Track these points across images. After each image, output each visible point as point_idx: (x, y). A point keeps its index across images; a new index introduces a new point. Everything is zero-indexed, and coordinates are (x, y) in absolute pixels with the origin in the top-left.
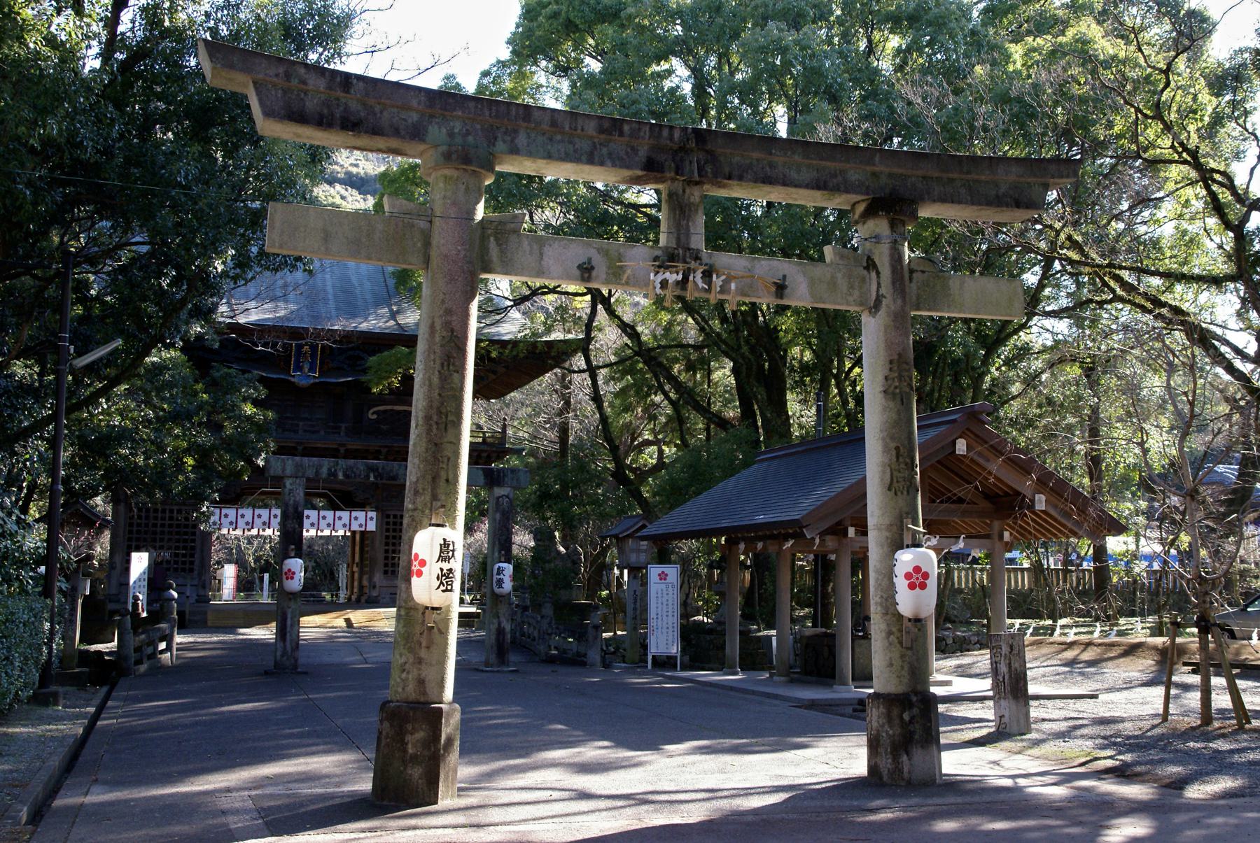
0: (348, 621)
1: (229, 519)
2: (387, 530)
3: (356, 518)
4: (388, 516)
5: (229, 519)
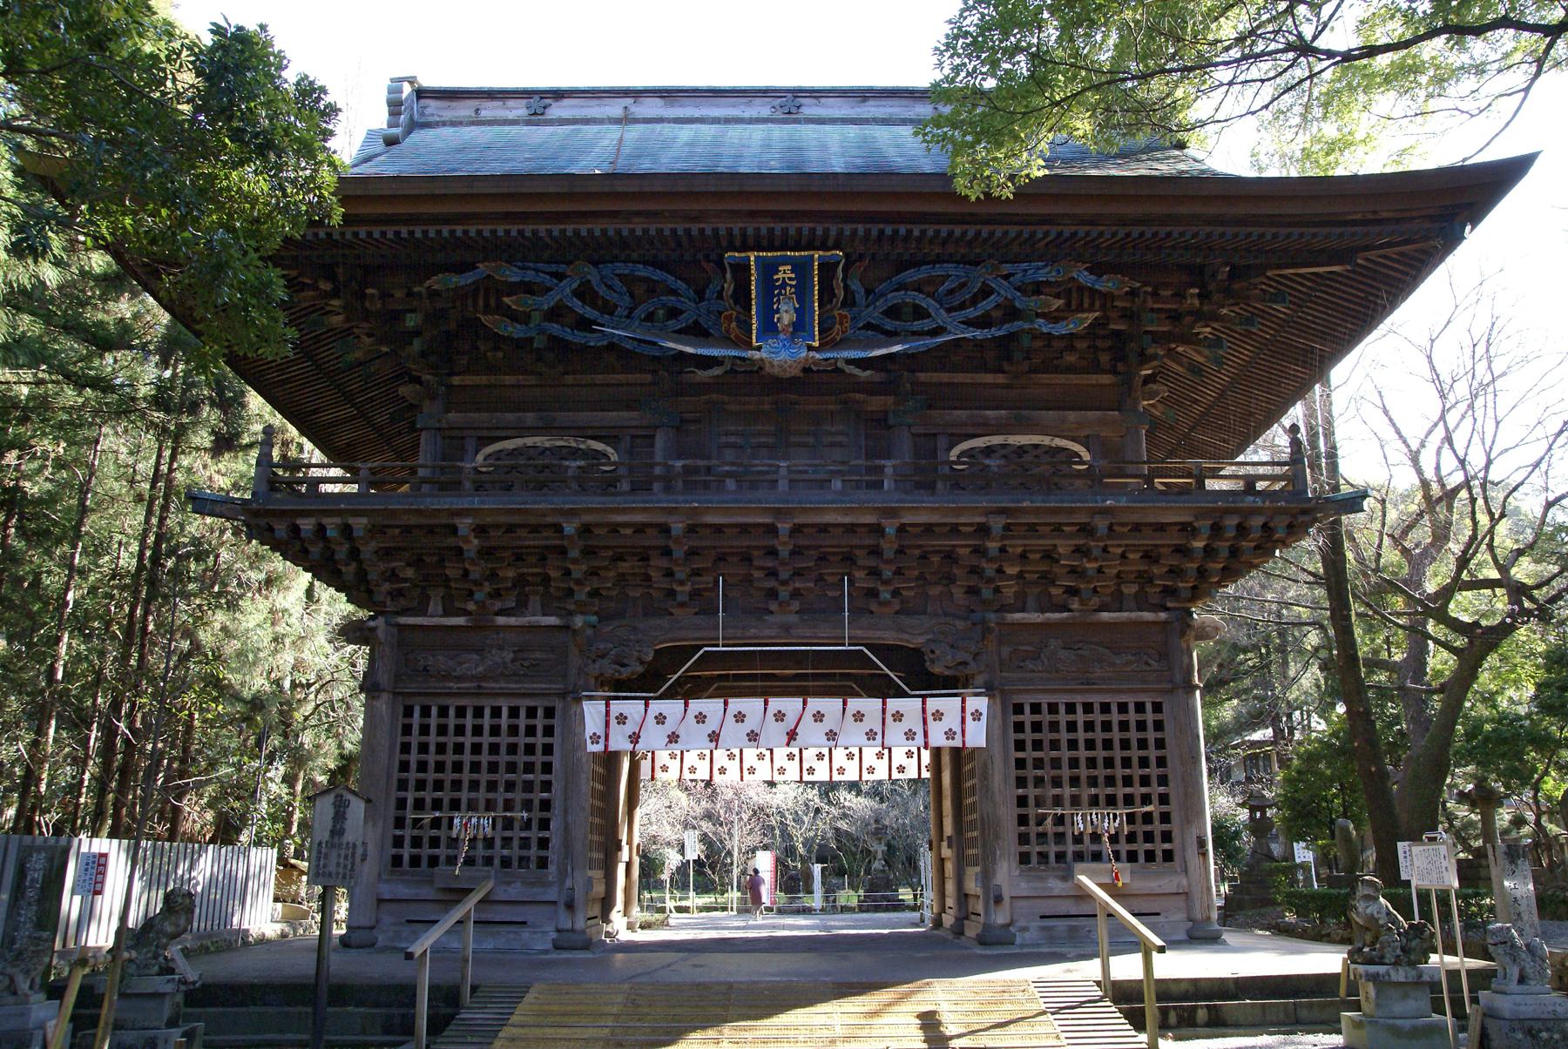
2: (1020, 745)
4: (1019, 709)
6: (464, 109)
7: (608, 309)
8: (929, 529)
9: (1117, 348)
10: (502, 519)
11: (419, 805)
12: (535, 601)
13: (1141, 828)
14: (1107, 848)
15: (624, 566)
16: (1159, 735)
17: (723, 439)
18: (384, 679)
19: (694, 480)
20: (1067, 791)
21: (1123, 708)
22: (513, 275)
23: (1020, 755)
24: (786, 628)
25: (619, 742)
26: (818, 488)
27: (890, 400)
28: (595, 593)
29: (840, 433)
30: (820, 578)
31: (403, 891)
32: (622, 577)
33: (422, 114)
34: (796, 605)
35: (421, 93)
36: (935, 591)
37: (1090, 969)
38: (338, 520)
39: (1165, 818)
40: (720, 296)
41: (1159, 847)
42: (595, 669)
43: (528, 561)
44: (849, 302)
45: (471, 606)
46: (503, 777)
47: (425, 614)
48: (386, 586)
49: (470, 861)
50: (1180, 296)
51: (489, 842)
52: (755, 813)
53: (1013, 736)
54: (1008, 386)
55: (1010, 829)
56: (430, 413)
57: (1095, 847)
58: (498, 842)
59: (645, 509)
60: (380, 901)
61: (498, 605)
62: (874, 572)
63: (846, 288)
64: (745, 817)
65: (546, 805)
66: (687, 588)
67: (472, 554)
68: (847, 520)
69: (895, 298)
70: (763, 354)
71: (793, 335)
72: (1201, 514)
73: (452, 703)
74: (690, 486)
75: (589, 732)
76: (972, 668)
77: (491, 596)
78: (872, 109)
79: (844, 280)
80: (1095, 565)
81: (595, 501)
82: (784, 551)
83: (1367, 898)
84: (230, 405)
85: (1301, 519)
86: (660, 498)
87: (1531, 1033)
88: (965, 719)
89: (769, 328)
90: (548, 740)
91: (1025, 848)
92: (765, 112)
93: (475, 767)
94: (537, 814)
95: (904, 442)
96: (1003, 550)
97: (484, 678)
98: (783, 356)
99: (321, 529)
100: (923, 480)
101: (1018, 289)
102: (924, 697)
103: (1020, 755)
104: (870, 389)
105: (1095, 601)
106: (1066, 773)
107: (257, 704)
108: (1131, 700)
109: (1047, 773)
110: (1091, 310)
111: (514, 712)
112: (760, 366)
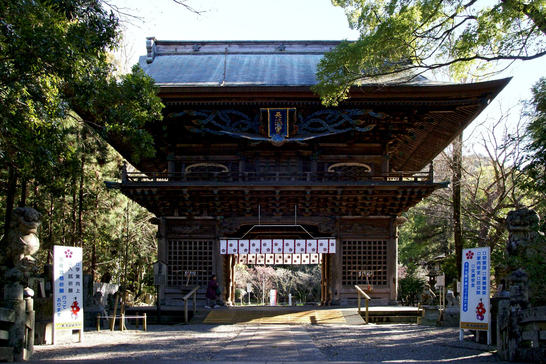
0: (313, 319)
1: (244, 247)
2: (344, 253)
3: (321, 244)
4: (345, 243)
5: (244, 247)
6: (171, 49)
7: (224, 124)
8: (320, 192)
9: (382, 136)
10: (196, 189)
11: (175, 268)
12: (205, 212)
13: (377, 276)
14: (368, 281)
15: (231, 202)
16: (385, 250)
17: (260, 164)
18: (163, 234)
19: (251, 178)
20: (357, 265)
21: (375, 243)
22: (195, 113)
23: (344, 255)
24: (278, 220)
25: (230, 251)
26: (287, 180)
27: (311, 152)
28: (222, 210)
29: (295, 162)
30: (288, 206)
31: (172, 291)
32: (230, 205)
33: (158, 51)
34: (281, 213)
35: (157, 43)
36: (322, 209)
37: (357, 309)
38: (148, 189)
39: (385, 273)
40: (258, 120)
41: (383, 281)
42: (223, 231)
43: (202, 201)
44: (298, 122)
45: (187, 214)
46: (198, 261)
47: (173, 216)
48: (162, 208)
49: (190, 283)
50: (402, 119)
51: (195, 278)
52: (270, 278)
53: (342, 250)
54: (348, 148)
55: (340, 276)
56: (170, 156)
57: (364, 280)
58: (198, 278)
59: (238, 186)
60: (166, 293)
61: (195, 213)
62: (304, 204)
63: (298, 118)
64: (267, 280)
65: (211, 268)
66: (250, 208)
67: (187, 199)
68: (296, 189)
69: (313, 120)
70: (272, 140)
71: (281, 134)
72: (401, 188)
73: (183, 241)
74: (250, 180)
75: (221, 248)
76: (332, 231)
77: (192, 211)
78: (309, 49)
79: (297, 115)
80: (368, 202)
81: (223, 184)
82: (278, 198)
83: (426, 289)
84: (103, 150)
85: (430, 189)
86: (241, 183)
87: (452, 316)
88: (329, 246)
89: (274, 131)
90: (210, 251)
91: (344, 280)
92: (273, 50)
93: (190, 258)
94: (208, 271)
95: (314, 166)
96: (341, 198)
97: (191, 234)
98: (278, 140)
99: (143, 192)
100: (321, 176)
101: (350, 117)
102: (317, 240)
103: (344, 255)
104: (304, 148)
105: (369, 212)
106: (357, 260)
107: (117, 242)
108: (377, 240)
109: (352, 261)
110: (373, 124)
111: (200, 243)
112: (270, 144)
